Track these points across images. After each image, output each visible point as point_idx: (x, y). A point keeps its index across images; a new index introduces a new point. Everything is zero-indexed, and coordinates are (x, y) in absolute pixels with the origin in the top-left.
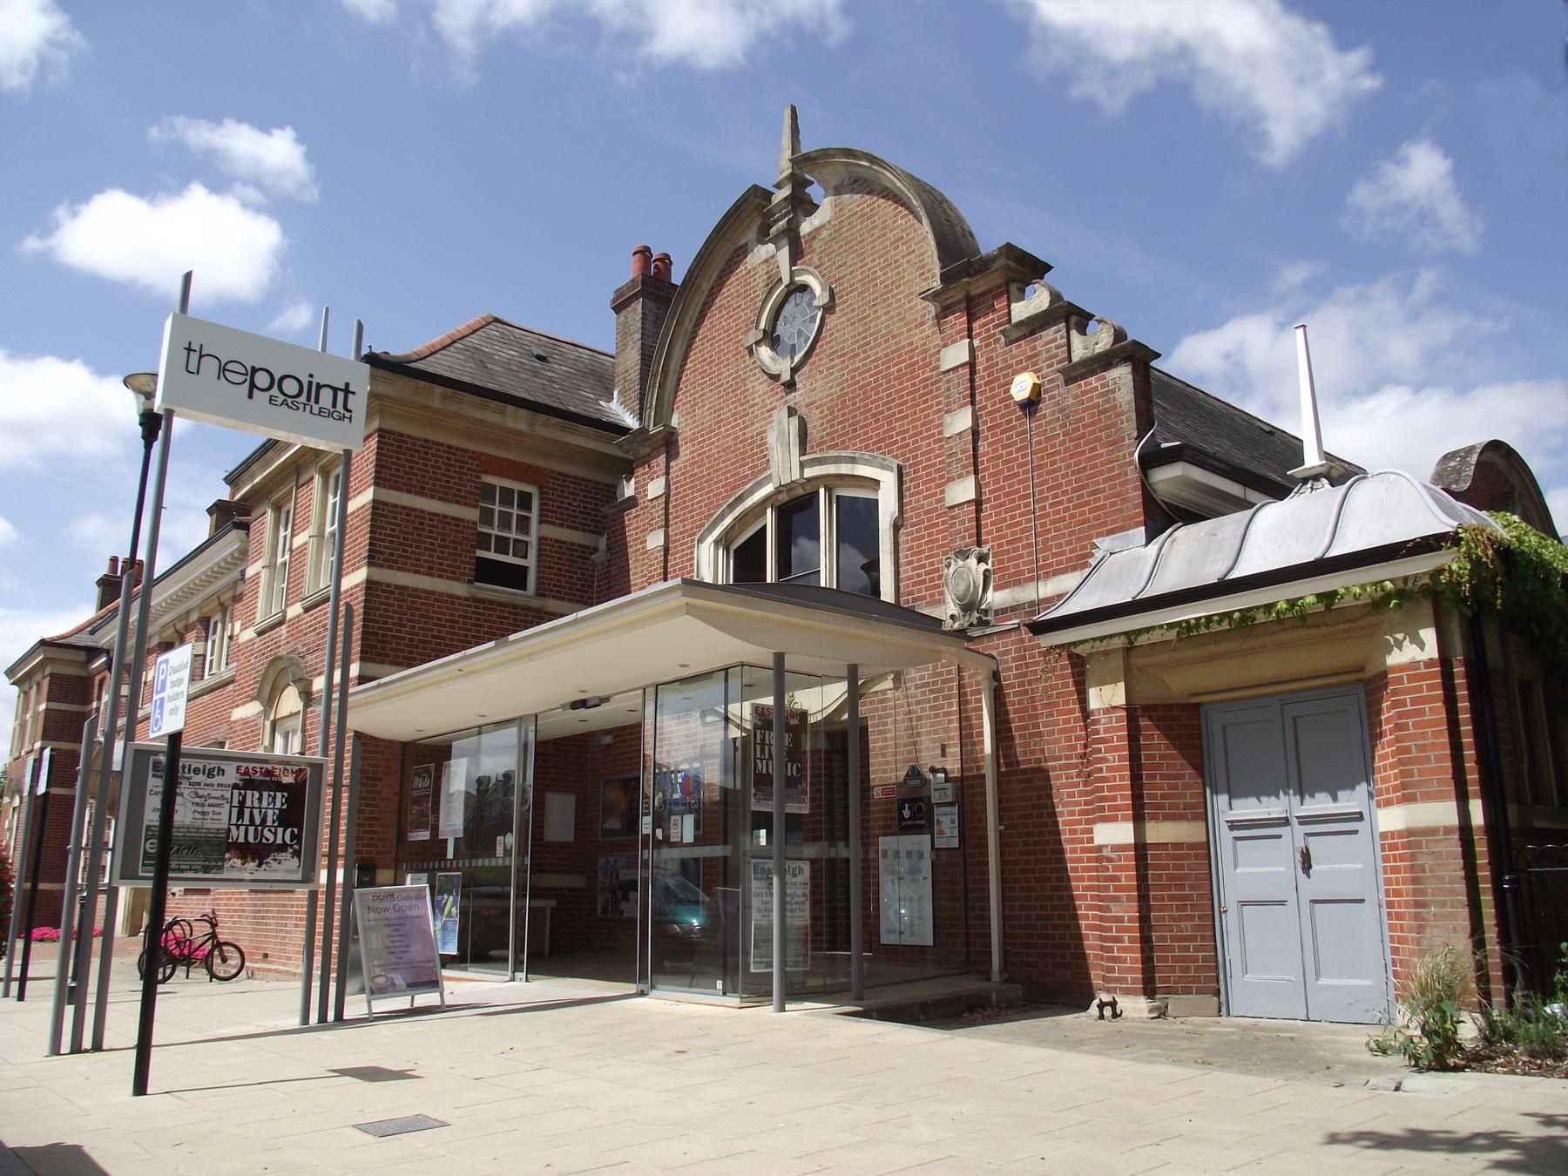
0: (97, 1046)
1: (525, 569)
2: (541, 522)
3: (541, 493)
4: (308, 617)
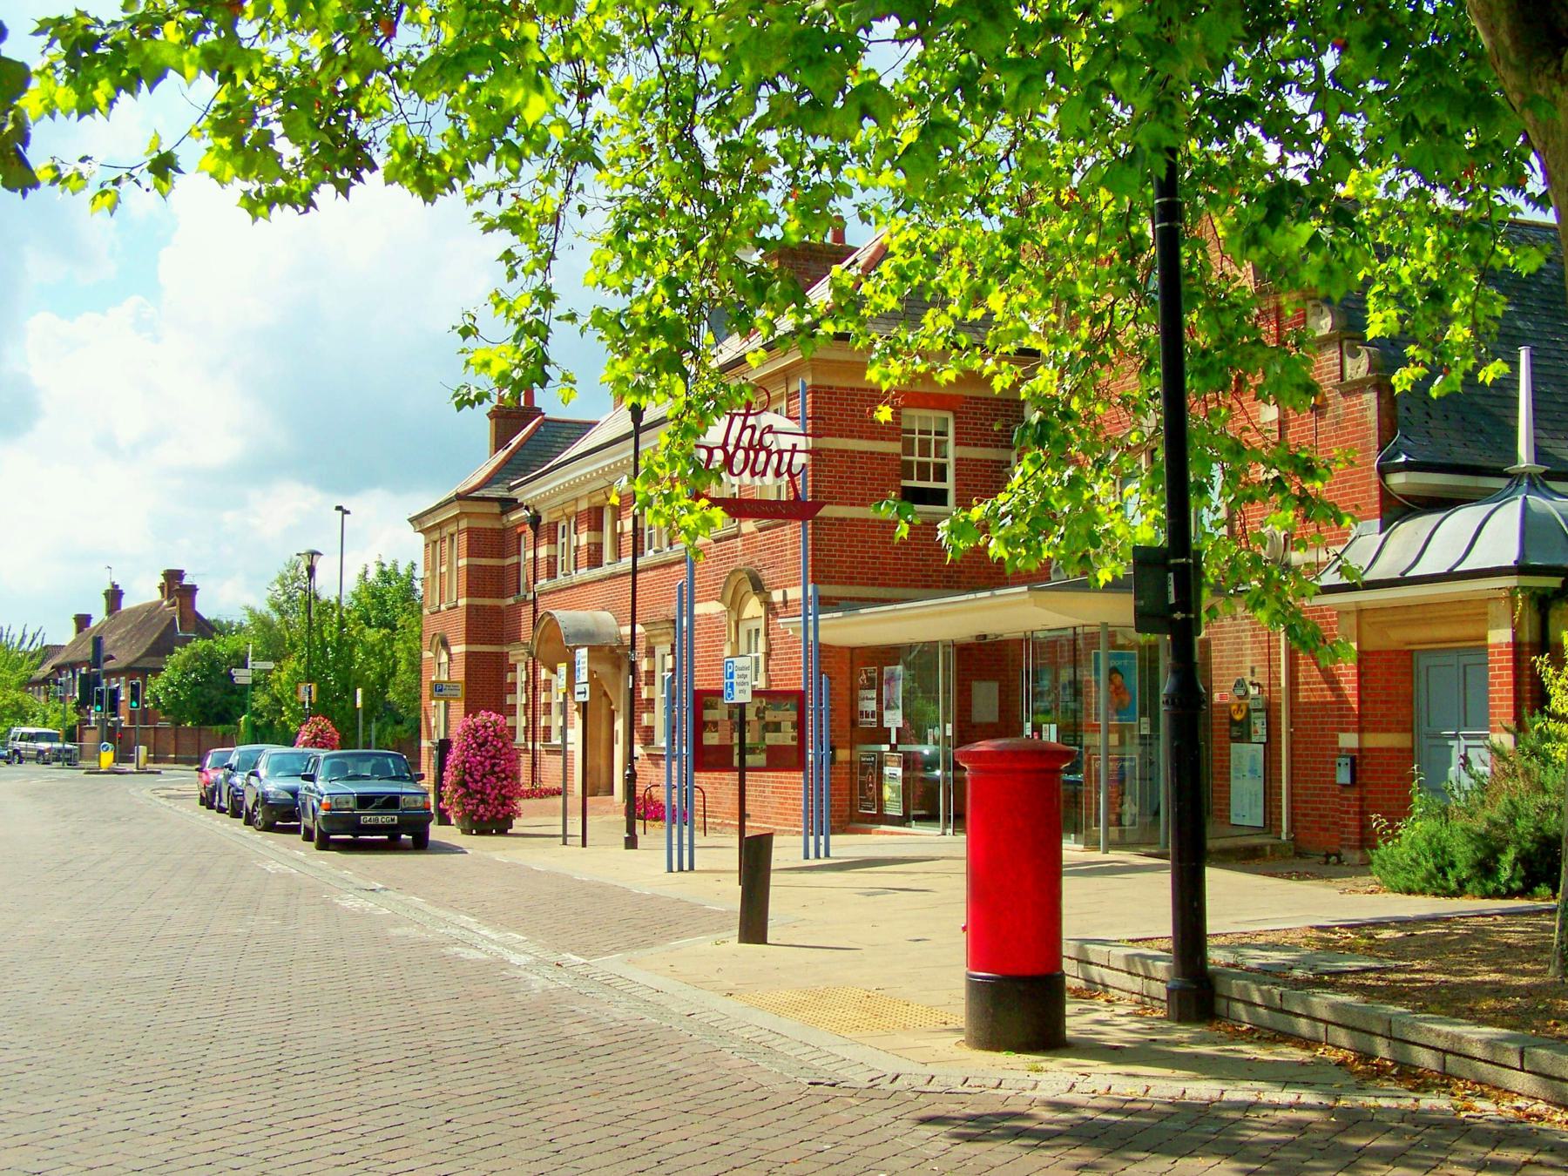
0: (691, 868)
1: (945, 491)
2: (957, 444)
3: (956, 418)
4: (761, 536)
